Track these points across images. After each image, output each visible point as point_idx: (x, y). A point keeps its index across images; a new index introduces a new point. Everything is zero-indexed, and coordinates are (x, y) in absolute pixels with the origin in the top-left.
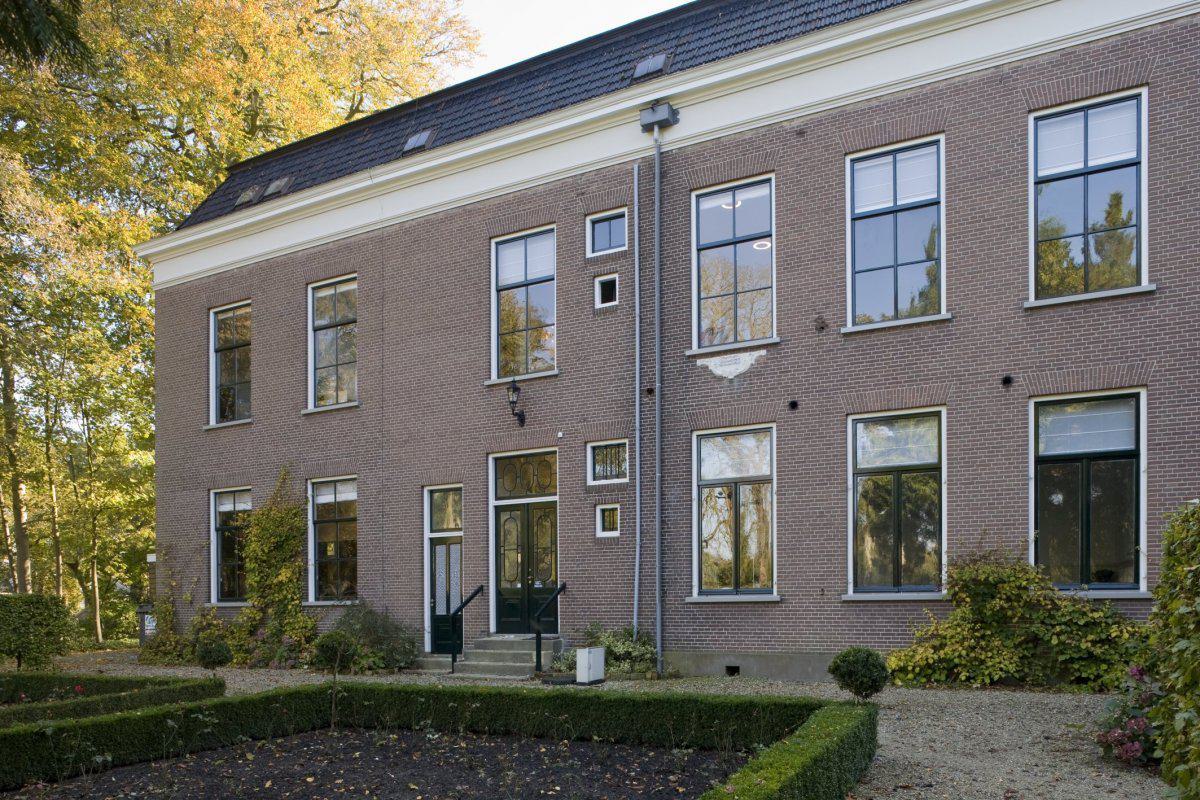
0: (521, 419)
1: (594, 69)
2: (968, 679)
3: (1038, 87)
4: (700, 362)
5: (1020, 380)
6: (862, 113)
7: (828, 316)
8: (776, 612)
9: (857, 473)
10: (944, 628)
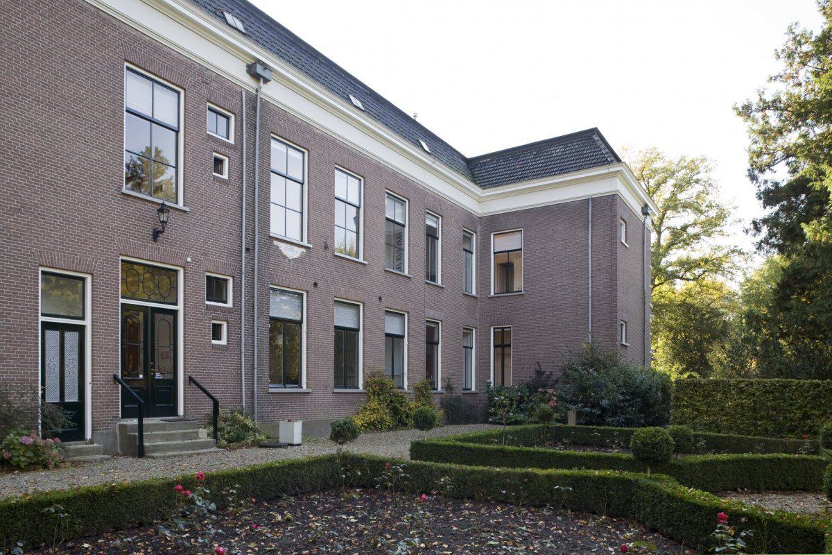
0: (156, 235)
4: (275, 243)
8: (307, 398)
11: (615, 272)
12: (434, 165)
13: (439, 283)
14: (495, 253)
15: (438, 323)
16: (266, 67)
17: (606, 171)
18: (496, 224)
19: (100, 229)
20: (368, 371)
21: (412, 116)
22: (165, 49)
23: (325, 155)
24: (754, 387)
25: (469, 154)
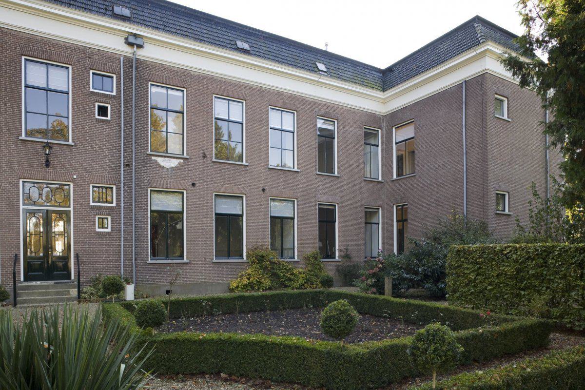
0: (47, 164)
1: (186, 26)
2: (258, 288)
3: (55, 53)
4: (153, 158)
5: (267, 190)
6: (220, 81)
7: (207, 153)
8: (186, 266)
9: (152, 211)
10: (249, 271)
11: (486, 146)
12: (320, 80)
13: (336, 173)
14: (396, 144)
15: (335, 206)
16: (136, 36)
17: (474, 54)
18: (396, 119)
19: (4, 164)
20: (250, 246)
21: (323, 48)
22: (53, 42)
23: (202, 89)
24: (519, 253)
25: (383, 65)
